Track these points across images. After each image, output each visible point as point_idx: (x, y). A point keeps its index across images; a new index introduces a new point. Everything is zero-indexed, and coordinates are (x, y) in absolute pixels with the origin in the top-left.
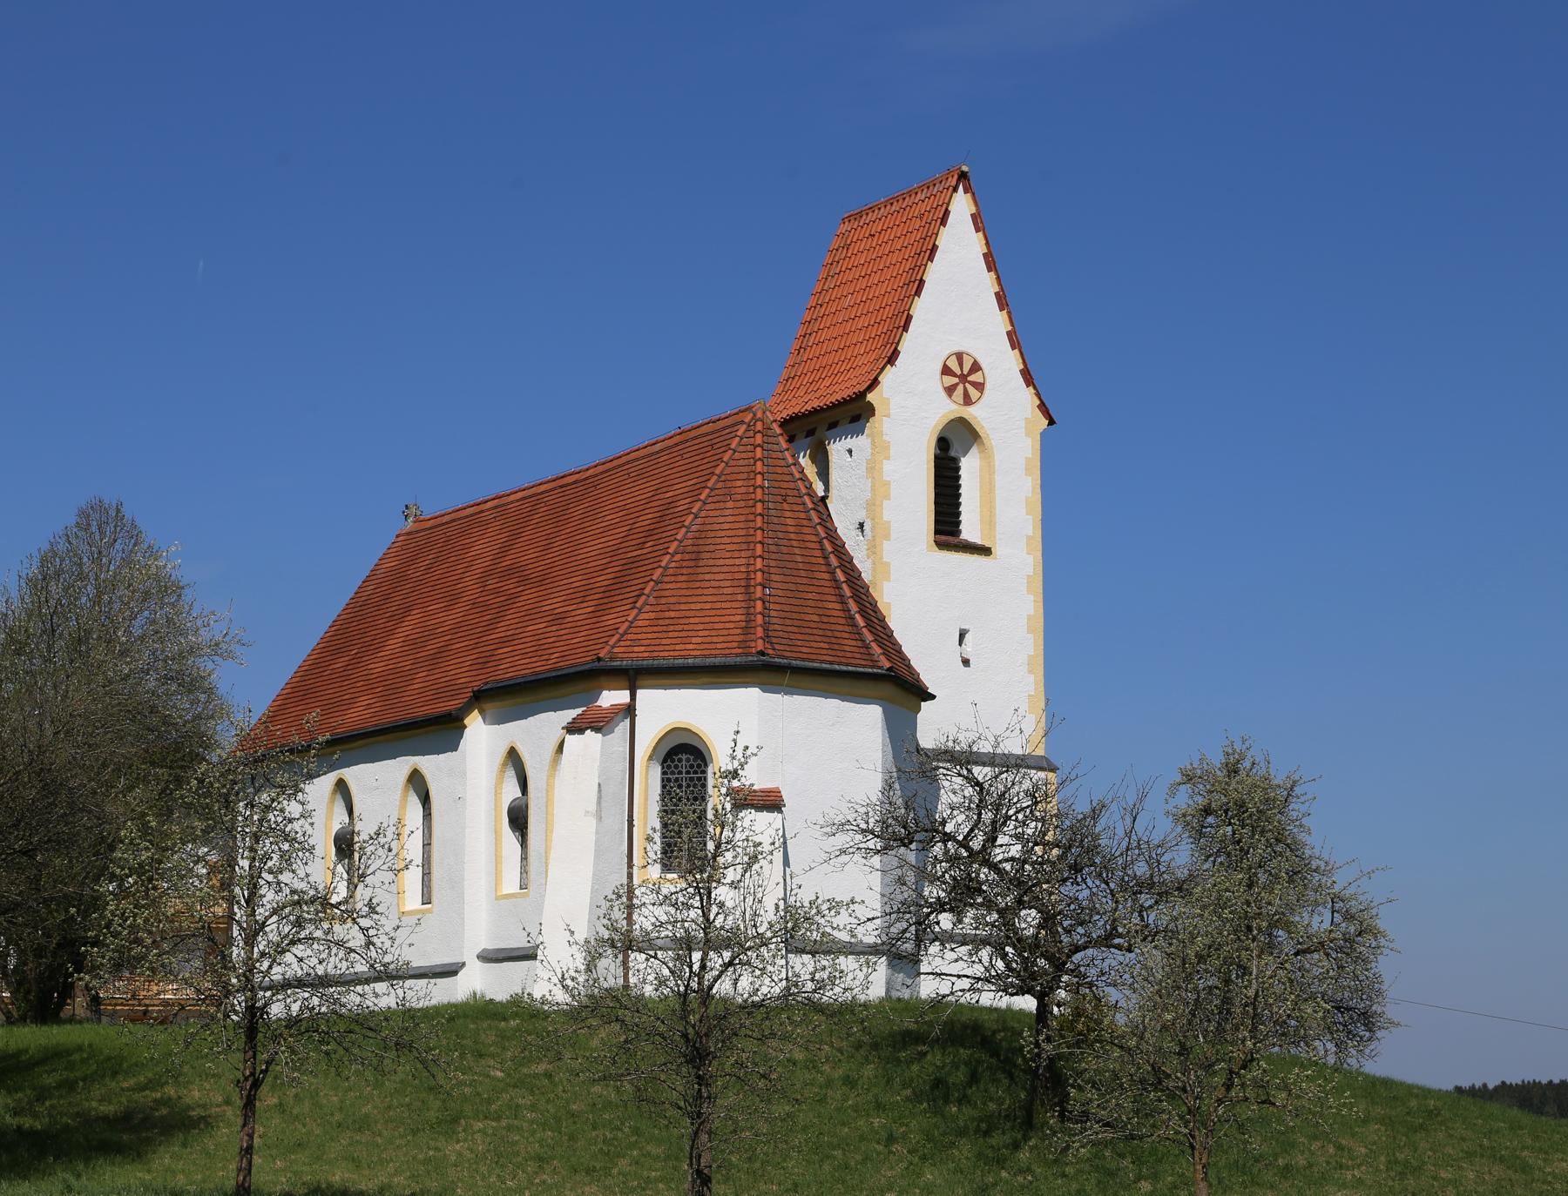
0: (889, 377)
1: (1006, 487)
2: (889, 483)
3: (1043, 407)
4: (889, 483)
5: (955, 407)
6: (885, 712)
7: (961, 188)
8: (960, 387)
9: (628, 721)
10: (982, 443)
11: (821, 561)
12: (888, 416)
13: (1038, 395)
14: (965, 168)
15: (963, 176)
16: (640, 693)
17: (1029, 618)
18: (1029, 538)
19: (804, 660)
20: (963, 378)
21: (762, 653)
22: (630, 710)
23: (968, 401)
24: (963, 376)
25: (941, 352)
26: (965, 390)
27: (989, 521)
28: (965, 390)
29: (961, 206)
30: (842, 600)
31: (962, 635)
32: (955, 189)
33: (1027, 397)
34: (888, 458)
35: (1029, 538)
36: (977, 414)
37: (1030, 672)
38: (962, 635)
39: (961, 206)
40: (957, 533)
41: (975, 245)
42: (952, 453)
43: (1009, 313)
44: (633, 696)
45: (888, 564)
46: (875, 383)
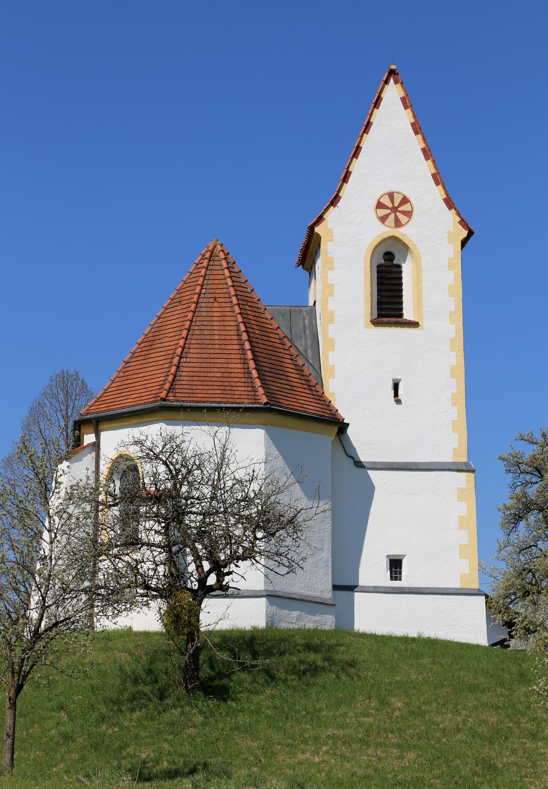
0: (332, 215)
1: (434, 281)
2: (333, 285)
3: (463, 223)
4: (333, 285)
5: (387, 229)
6: (268, 433)
7: (392, 81)
8: (399, 215)
9: (94, 454)
10: (412, 252)
11: (235, 337)
12: (332, 240)
13: (459, 214)
14: (393, 67)
15: (392, 73)
16: (104, 435)
17: (452, 368)
18: (451, 313)
19: (197, 402)
20: (394, 209)
21: (164, 400)
22: (96, 446)
23: (398, 224)
24: (394, 208)
25: (378, 191)
26: (396, 217)
27: (418, 305)
28: (396, 217)
29: (393, 93)
30: (245, 362)
31: (396, 387)
32: (387, 82)
33: (450, 218)
34: (332, 269)
35: (451, 313)
36: (407, 233)
37: (453, 405)
38: (396, 387)
39: (393, 93)
40: (401, 316)
41: (406, 117)
42: (395, 262)
43: (434, 161)
44: (98, 437)
45: (333, 340)
46: (320, 219)
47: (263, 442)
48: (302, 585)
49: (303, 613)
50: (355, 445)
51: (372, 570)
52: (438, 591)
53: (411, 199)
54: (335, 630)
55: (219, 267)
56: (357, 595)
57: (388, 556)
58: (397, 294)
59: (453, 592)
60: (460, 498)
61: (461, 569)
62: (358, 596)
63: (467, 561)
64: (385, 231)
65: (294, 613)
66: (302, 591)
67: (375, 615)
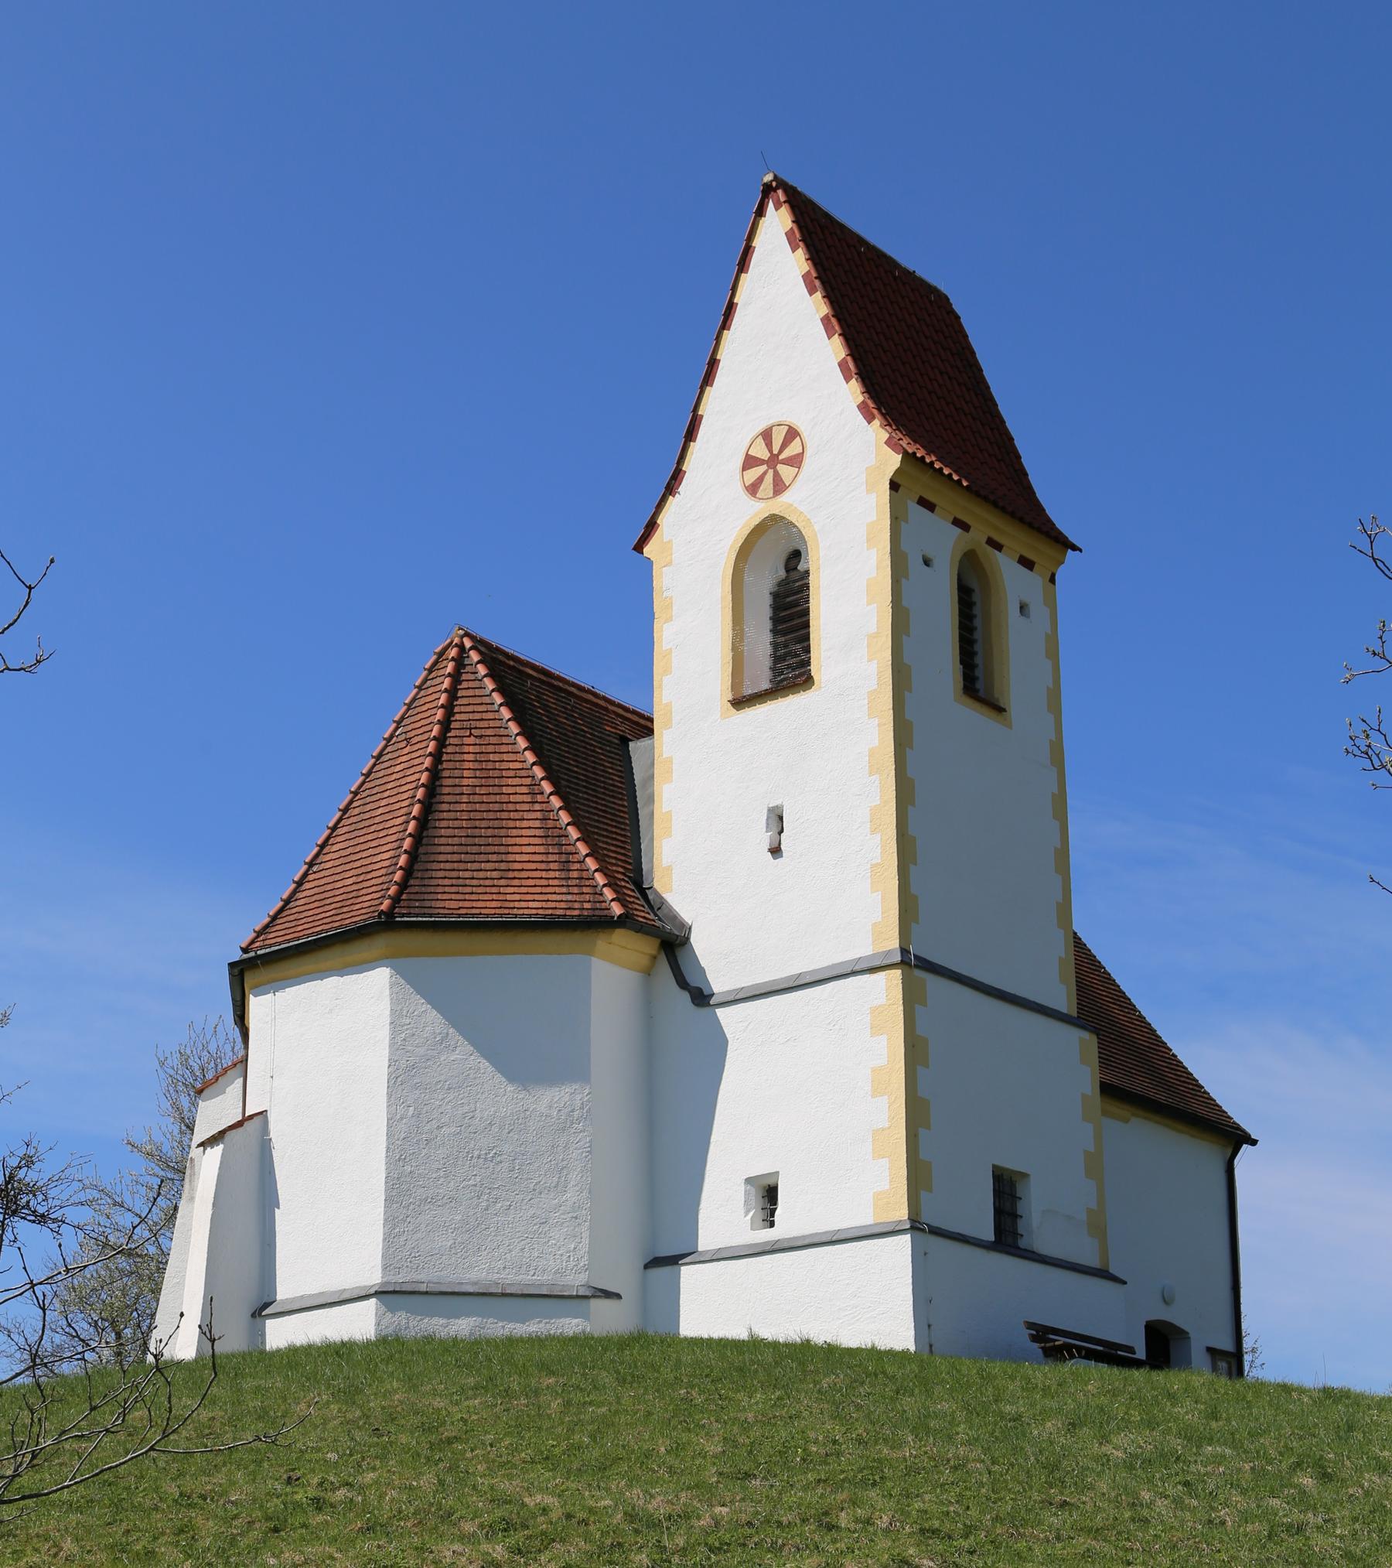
6: (398, 971)
14: (768, 178)
17: (872, 753)
23: (779, 487)
32: (760, 212)
47: (387, 992)
48: (500, 1264)
49: (491, 1320)
50: (703, 963)
51: (722, 1214)
52: (816, 1240)
53: (804, 434)
54: (196, 1360)
55: (472, 677)
56: (374, 1277)
57: (749, 1181)
58: (803, 632)
59: (824, 1239)
60: (876, 1029)
61: (877, 1184)
62: (688, 1273)
63: (885, 1162)
64: (754, 511)
65: (460, 1322)
66: (496, 1276)
67: (714, 1305)
